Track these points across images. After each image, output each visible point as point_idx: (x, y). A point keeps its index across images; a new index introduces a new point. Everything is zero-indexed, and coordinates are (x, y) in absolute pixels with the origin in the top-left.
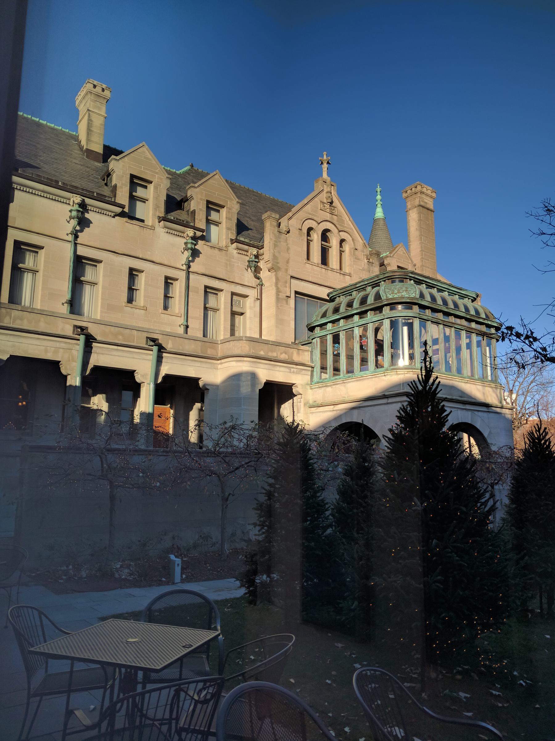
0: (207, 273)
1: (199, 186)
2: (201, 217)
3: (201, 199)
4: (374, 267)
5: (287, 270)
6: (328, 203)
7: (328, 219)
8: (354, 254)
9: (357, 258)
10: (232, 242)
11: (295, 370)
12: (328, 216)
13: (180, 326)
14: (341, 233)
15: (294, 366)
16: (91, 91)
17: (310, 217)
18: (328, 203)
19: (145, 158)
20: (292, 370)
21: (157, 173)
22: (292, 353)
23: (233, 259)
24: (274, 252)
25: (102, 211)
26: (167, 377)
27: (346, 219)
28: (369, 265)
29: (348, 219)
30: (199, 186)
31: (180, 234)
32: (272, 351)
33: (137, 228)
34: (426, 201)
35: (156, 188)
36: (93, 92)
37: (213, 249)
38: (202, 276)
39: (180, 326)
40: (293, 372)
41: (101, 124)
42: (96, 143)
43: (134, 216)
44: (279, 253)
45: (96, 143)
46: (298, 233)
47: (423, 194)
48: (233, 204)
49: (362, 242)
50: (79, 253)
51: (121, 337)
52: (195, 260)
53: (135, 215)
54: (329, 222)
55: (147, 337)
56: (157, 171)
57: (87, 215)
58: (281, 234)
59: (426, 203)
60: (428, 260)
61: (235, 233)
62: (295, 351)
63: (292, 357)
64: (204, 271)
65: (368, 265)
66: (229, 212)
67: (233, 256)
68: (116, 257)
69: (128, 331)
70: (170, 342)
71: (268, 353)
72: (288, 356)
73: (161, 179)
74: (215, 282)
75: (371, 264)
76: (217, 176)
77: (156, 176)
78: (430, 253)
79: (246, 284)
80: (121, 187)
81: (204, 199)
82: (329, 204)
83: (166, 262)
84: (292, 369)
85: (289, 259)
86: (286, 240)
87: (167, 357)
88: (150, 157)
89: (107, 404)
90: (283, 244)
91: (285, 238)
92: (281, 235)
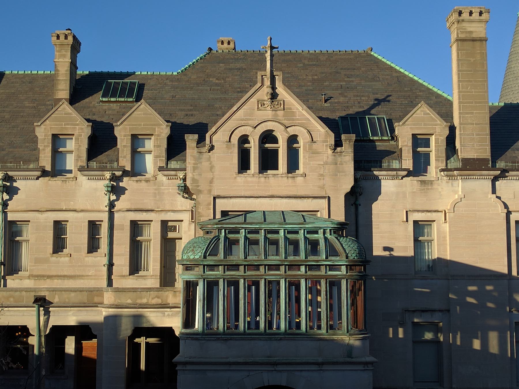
0: (133, 207)
1: (122, 123)
2: (125, 154)
3: (125, 136)
4: (344, 156)
5: (210, 191)
6: (269, 99)
7: (270, 118)
8: (310, 148)
9: (316, 153)
10: (161, 169)
11: (170, 313)
12: (268, 113)
13: (104, 265)
14: (288, 129)
15: (168, 310)
16: (55, 43)
17: (243, 123)
18: (269, 99)
19: (65, 114)
20: (166, 313)
21: (78, 125)
22: (167, 297)
23: (163, 186)
24: (194, 176)
25: (26, 178)
26: (54, 328)
27: (298, 109)
28: (335, 155)
29: (300, 109)
30: (122, 123)
31: (101, 178)
32: (141, 298)
33: (59, 183)
34: (469, 29)
35: (77, 139)
36: (57, 43)
37: (139, 182)
38: (128, 212)
39: (104, 265)
40: (168, 315)
41: (67, 71)
42: (63, 90)
43: (63, 169)
44: (200, 175)
45: (63, 90)
46: (225, 146)
47: (464, 22)
48: (162, 129)
49: (324, 130)
50: (9, 219)
51: (12, 299)
52: (121, 198)
53: (66, 167)
54: (271, 121)
55: (34, 296)
56: (77, 123)
57: (15, 184)
58: (202, 153)
59: (471, 32)
60: (472, 113)
61: (164, 159)
62: (171, 293)
63: (167, 300)
64: (128, 207)
65: (333, 157)
66: (157, 139)
67: (163, 184)
68: (41, 214)
69: (17, 293)
70: (57, 296)
71: (136, 300)
72: (162, 300)
73: (82, 129)
74: (142, 214)
75: (339, 153)
76: (141, 107)
77: (76, 127)
78: (476, 103)
79: (179, 208)
80: (44, 150)
81: (128, 135)
82: (270, 100)
83: (89, 208)
84: (165, 313)
85: (213, 178)
86: (209, 159)
87: (54, 311)
88: (71, 112)
89: (68, 337)
90: (205, 164)
91: (208, 156)
92: (203, 154)
